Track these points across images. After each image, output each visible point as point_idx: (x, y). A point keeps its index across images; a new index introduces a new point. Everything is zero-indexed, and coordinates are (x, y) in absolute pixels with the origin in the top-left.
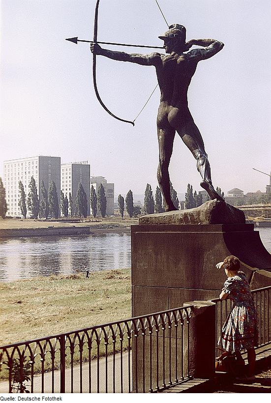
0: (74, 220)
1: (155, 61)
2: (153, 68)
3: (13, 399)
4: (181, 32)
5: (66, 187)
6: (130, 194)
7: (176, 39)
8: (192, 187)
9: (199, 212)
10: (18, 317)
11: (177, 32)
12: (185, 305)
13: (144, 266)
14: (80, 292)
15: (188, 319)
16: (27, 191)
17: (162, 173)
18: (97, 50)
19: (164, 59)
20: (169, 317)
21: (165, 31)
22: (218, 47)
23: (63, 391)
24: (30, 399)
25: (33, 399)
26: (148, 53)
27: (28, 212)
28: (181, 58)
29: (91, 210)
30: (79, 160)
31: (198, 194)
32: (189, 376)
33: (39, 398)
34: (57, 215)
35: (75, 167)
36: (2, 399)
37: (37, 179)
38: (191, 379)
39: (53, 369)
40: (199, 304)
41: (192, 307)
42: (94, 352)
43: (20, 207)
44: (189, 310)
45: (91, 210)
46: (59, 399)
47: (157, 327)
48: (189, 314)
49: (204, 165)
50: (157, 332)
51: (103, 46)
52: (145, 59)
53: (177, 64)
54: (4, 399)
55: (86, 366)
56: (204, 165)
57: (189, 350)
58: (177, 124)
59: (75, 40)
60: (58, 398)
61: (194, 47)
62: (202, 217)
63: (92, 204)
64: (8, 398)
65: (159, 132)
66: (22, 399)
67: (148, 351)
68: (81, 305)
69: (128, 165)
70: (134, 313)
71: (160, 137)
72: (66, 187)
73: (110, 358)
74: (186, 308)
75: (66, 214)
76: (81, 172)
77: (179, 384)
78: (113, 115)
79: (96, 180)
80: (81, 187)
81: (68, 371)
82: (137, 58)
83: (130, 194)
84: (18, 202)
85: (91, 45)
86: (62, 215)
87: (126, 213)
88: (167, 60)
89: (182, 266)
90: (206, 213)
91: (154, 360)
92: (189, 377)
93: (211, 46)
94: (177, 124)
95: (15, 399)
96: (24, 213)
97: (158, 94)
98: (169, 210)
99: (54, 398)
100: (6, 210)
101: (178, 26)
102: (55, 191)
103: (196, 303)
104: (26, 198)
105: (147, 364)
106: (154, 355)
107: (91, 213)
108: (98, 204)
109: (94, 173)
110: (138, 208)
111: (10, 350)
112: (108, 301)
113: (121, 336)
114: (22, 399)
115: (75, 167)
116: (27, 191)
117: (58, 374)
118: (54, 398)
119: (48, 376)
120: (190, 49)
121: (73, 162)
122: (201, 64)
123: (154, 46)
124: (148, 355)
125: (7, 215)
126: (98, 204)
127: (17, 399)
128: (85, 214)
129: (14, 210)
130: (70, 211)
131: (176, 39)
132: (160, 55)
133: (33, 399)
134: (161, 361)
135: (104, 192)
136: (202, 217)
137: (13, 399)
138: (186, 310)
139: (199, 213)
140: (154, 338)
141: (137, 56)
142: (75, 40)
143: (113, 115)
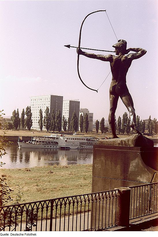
0: (69, 133)
1: (110, 59)
2: (109, 63)
3: (7, 235)
4: (124, 44)
5: (66, 114)
6: (103, 120)
7: (122, 48)
8: (139, 117)
9: (129, 140)
10: (35, 187)
11: (122, 44)
12: (115, 189)
13: (99, 166)
14: (70, 176)
15: (116, 196)
16: (44, 115)
17: (111, 118)
18: (80, 52)
19: (114, 58)
20: (92, 197)
21: (116, 43)
22: (144, 53)
23: (51, 230)
24: (18, 235)
25: (20, 235)
26: (106, 55)
27: (43, 127)
28: (123, 59)
29: (79, 128)
30: (74, 99)
31: (142, 121)
32: (115, 224)
33: (23, 234)
34: (60, 130)
35: (71, 102)
36: (1, 234)
37: (49, 108)
38: (117, 226)
39: (47, 219)
40: (122, 189)
41: (118, 190)
42: (75, 210)
43: (39, 124)
44: (117, 191)
45: (79, 128)
46: (35, 235)
47: (110, 197)
48: (117, 194)
49: (133, 115)
50: (113, 199)
51: (83, 50)
52: (105, 58)
53: (121, 61)
54: (2, 235)
55: (71, 217)
56: (133, 115)
57: (116, 212)
58: (120, 91)
59: (69, 46)
60: (34, 234)
61: (131, 52)
62: (130, 143)
63: (80, 125)
64: (5, 234)
65: (110, 96)
66: (13, 235)
67: (98, 211)
68: (71, 183)
69: (98, 105)
70: (93, 190)
71: (111, 99)
72: (66, 114)
73: (83, 214)
74: (115, 190)
75: (65, 129)
76: (74, 105)
77: (110, 228)
78: (87, 87)
79: (83, 110)
80: (75, 114)
81: (54, 220)
82: (101, 57)
83: (103, 120)
84: (38, 121)
85: (77, 49)
86: (62, 130)
87: (100, 131)
88: (116, 59)
89: (119, 167)
90: (132, 141)
91: (101, 216)
92: (115, 225)
93: (140, 52)
94: (120, 91)
95: (9, 235)
96: (41, 128)
97: (111, 76)
98: (114, 138)
99: (31, 234)
100: (31, 125)
101: (123, 41)
102: (60, 116)
103: (121, 188)
104: (43, 119)
105: (97, 218)
106: (101, 213)
107: (79, 130)
108: (84, 125)
109: (82, 107)
110: (107, 128)
111: (33, 205)
112: (85, 182)
113: (89, 201)
114: (13, 235)
115: (71, 102)
116: (44, 115)
117: (49, 221)
118: (31, 234)
119: (44, 222)
120: (129, 53)
121: (71, 100)
122: (134, 62)
123: (110, 51)
124: (97, 213)
125: (31, 128)
126: (84, 125)
127: (10, 235)
128: (76, 129)
129: (35, 125)
130: (67, 128)
131: (122, 48)
132: (112, 56)
133: (20, 235)
134: (104, 217)
135: (88, 117)
136: (130, 143)
137: (7, 235)
138: (115, 192)
139: (128, 140)
140: (101, 205)
141: (100, 56)
142: (69, 46)
143: (87, 87)
